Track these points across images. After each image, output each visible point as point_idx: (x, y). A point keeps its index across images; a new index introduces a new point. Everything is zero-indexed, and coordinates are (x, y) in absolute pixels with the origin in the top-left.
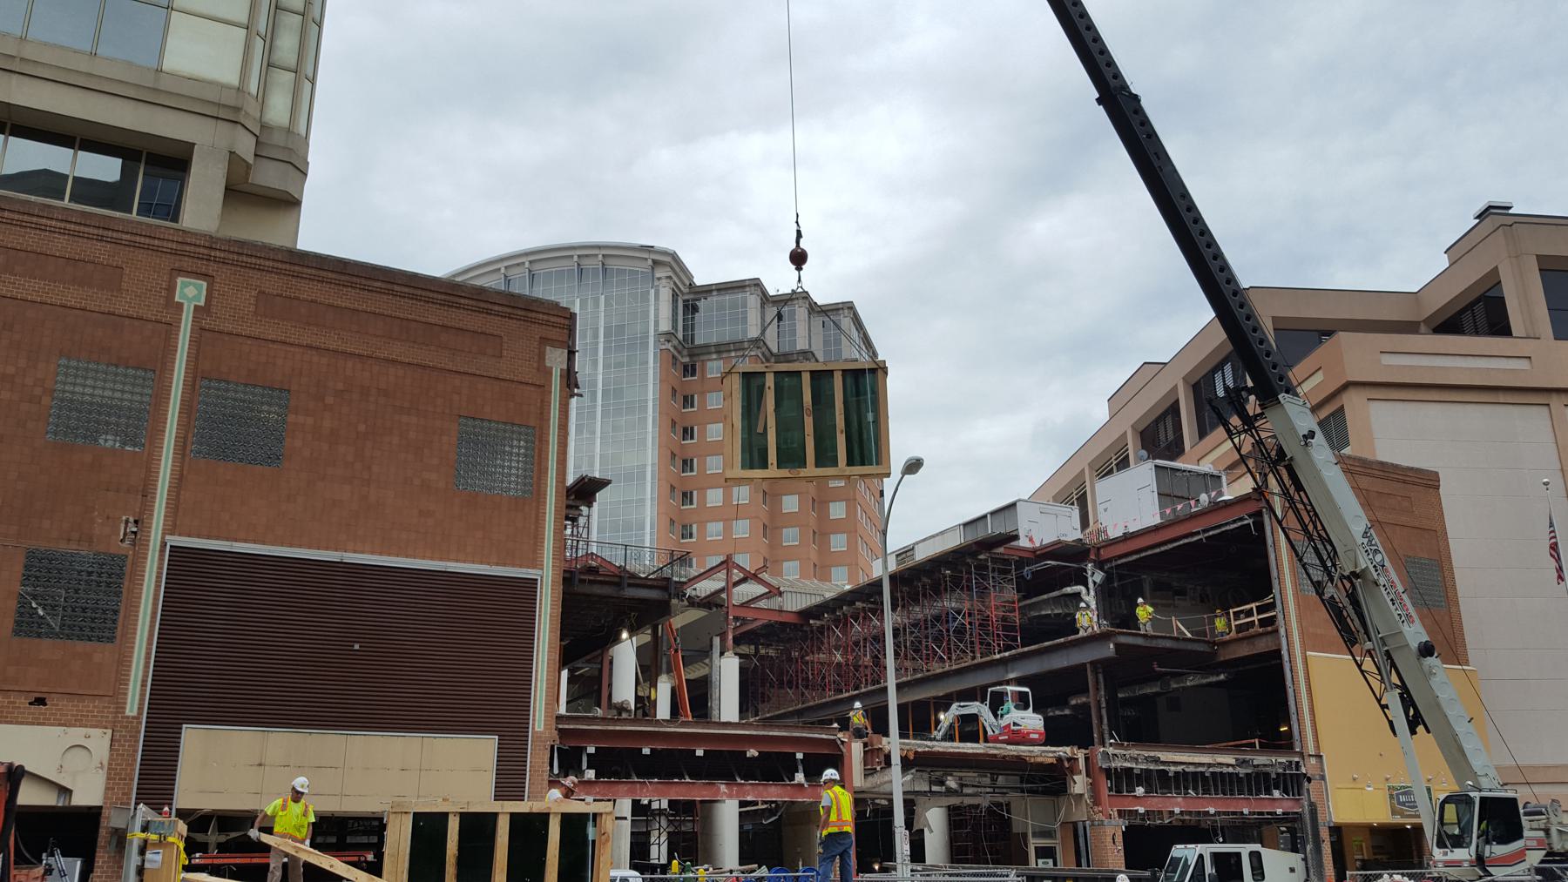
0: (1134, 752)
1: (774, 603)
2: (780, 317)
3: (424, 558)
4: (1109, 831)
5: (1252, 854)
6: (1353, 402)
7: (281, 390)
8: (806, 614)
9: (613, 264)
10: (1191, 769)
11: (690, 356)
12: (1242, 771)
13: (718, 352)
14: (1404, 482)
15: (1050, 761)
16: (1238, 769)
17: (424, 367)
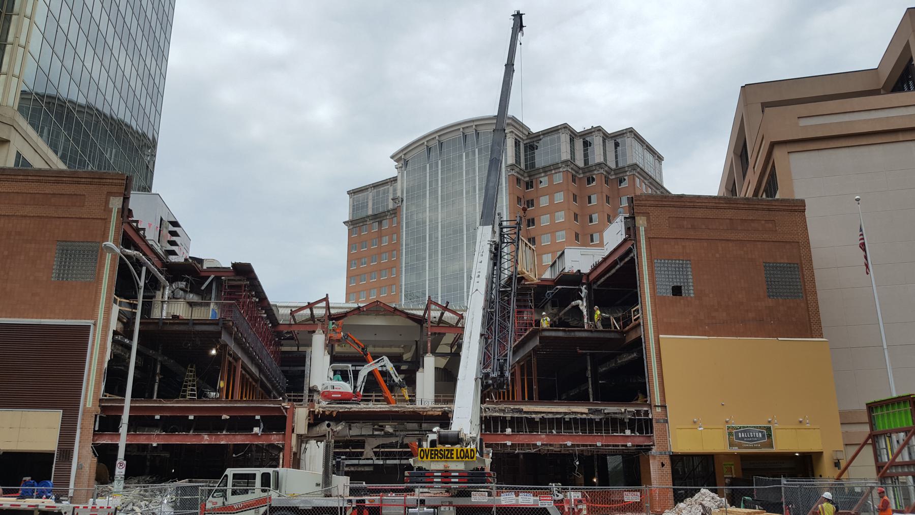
0: (502, 406)
10: (550, 416)
11: (529, 176)
12: (597, 417)
13: (545, 172)
14: (769, 210)
15: (437, 413)
16: (592, 416)
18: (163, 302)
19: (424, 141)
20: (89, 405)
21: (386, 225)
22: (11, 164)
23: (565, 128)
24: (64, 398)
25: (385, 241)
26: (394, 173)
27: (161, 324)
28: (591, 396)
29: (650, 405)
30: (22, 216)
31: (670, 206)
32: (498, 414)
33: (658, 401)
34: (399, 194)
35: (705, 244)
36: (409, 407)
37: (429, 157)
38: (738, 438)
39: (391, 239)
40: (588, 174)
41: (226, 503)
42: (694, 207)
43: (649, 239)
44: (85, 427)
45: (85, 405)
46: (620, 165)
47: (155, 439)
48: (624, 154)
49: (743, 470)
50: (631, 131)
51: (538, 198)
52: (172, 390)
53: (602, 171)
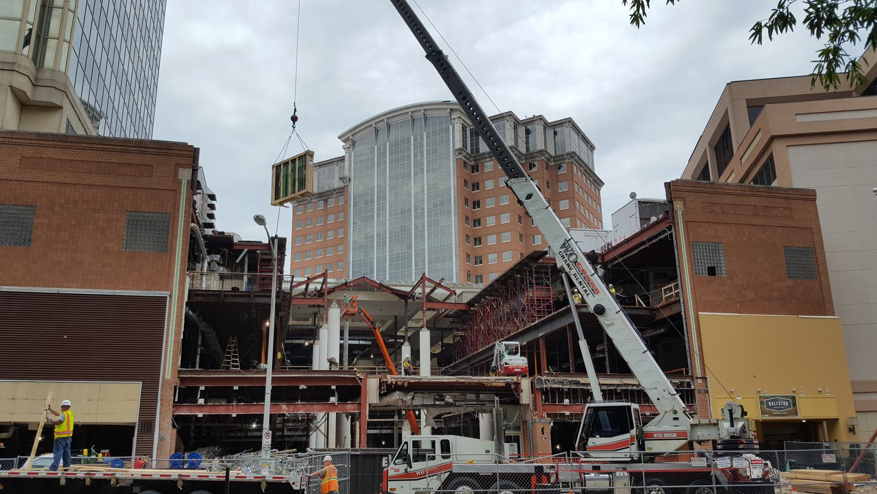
0: (561, 378)
1: (452, 299)
2: (555, 133)
3: (105, 289)
4: (539, 427)
5: (442, 441)
6: (778, 148)
7: (32, 206)
8: (470, 304)
9: (429, 114)
11: (475, 161)
14: (786, 198)
17: (108, 186)
18: (202, 274)
19: (373, 122)
20: (168, 376)
21: (331, 202)
22: (63, 131)
23: (510, 115)
24: (144, 370)
25: (331, 219)
26: (342, 153)
27: (222, 296)
28: (608, 369)
29: (692, 377)
30: (88, 185)
31: (703, 192)
32: (557, 386)
33: (699, 373)
34: (346, 174)
35: (734, 228)
36: (412, 378)
37: (377, 139)
38: (768, 407)
39: (337, 218)
40: (530, 160)
41: (409, 470)
42: (715, 193)
43: (686, 223)
44: (165, 397)
45: (164, 377)
46: (559, 153)
47: (200, 410)
48: (563, 142)
49: (764, 435)
50: (569, 121)
51: (483, 181)
52: (210, 363)
53: (543, 158)
